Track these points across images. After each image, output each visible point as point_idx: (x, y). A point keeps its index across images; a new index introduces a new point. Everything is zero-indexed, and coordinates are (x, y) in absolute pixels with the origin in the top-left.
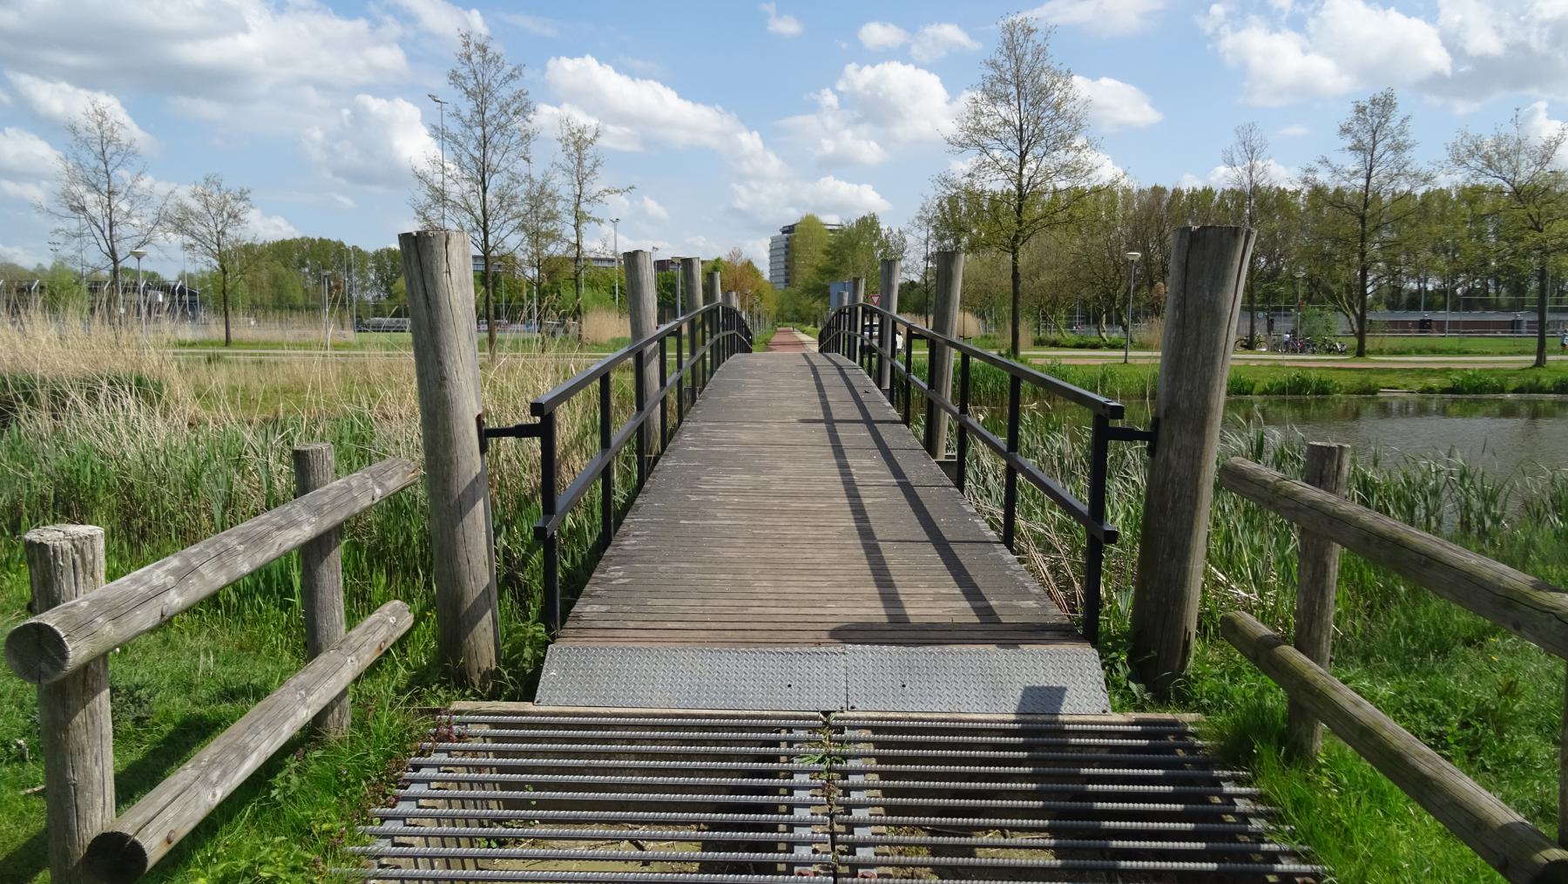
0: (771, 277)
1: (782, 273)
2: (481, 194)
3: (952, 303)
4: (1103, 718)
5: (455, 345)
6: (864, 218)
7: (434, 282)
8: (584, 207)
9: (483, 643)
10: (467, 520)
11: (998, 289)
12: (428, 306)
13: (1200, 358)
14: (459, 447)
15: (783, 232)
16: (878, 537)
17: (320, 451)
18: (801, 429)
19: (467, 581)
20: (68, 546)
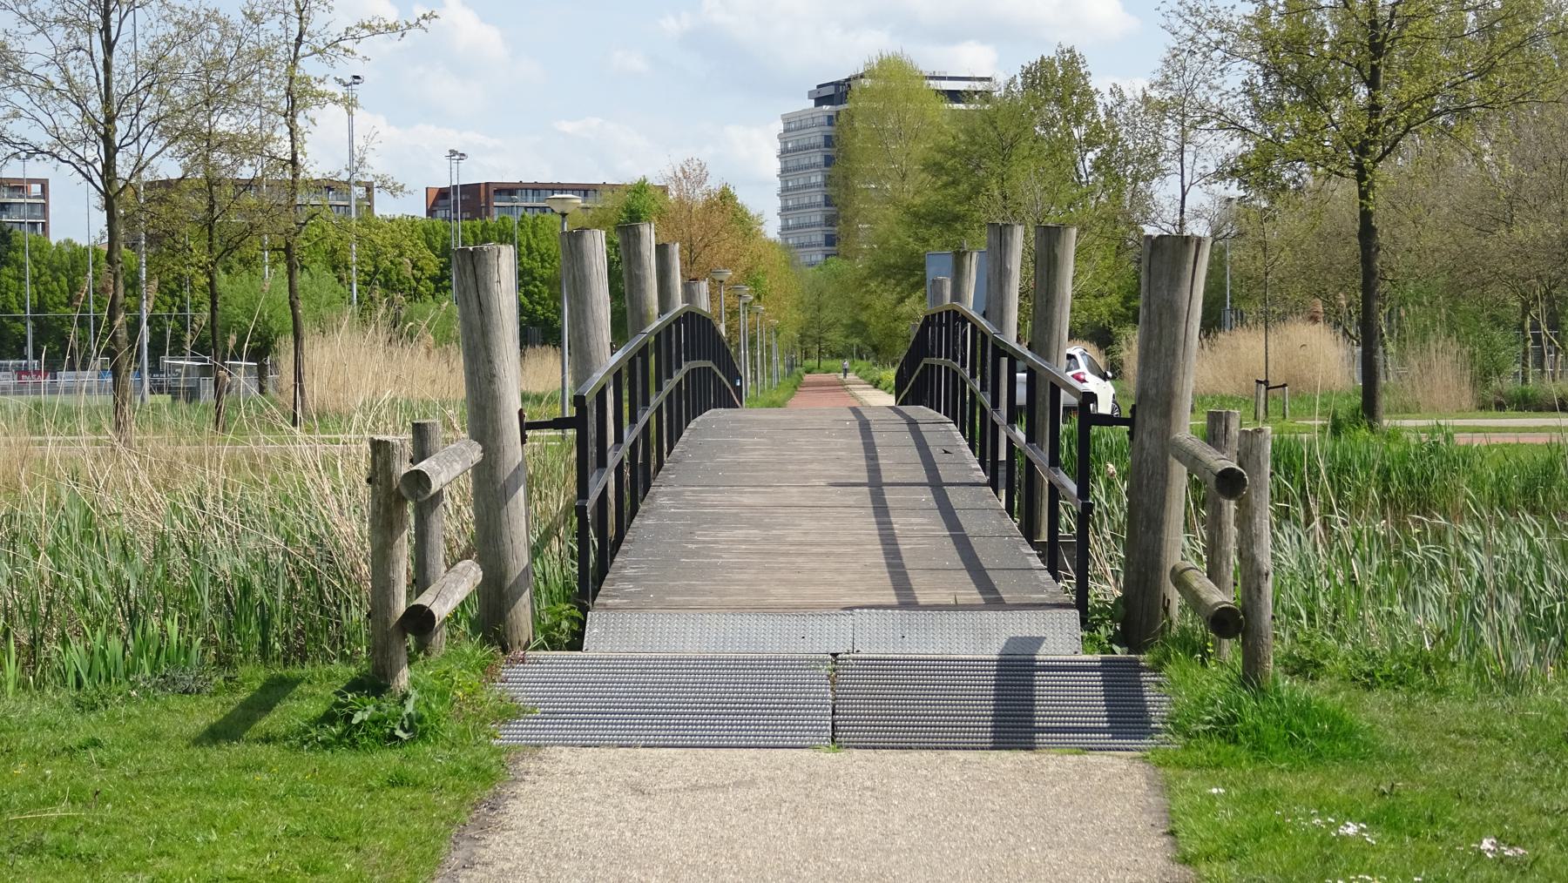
0: (785, 228)
1: (817, 217)
2: (99, 55)
3: (1058, 303)
4: (1072, 658)
5: (503, 346)
6: (1044, 64)
7: (487, 290)
8: (309, 67)
9: (523, 618)
10: (511, 503)
11: (1412, 257)
12: (481, 311)
13: (1163, 350)
14: (505, 437)
15: (820, 101)
16: (907, 567)
17: (435, 424)
18: (831, 492)
19: (510, 560)
20: (399, 443)
